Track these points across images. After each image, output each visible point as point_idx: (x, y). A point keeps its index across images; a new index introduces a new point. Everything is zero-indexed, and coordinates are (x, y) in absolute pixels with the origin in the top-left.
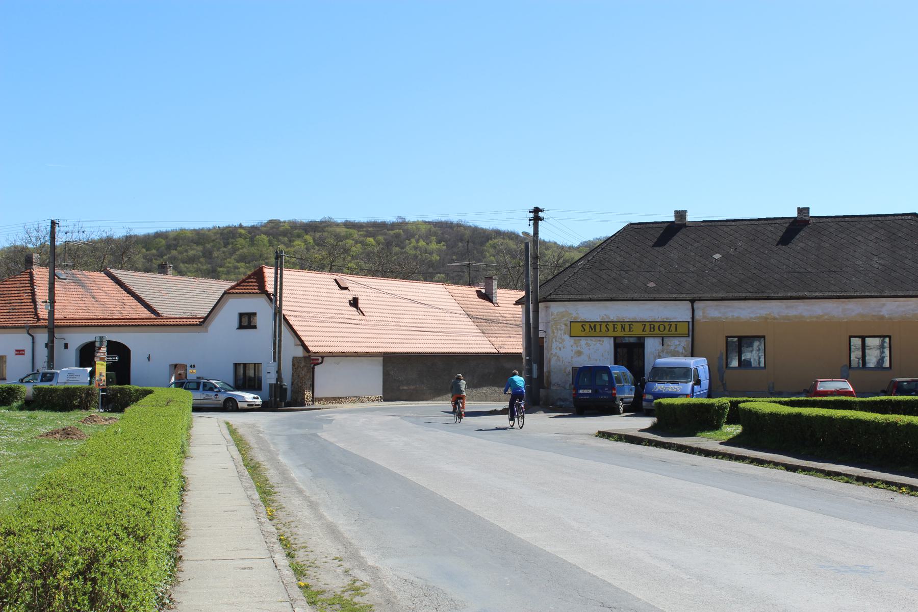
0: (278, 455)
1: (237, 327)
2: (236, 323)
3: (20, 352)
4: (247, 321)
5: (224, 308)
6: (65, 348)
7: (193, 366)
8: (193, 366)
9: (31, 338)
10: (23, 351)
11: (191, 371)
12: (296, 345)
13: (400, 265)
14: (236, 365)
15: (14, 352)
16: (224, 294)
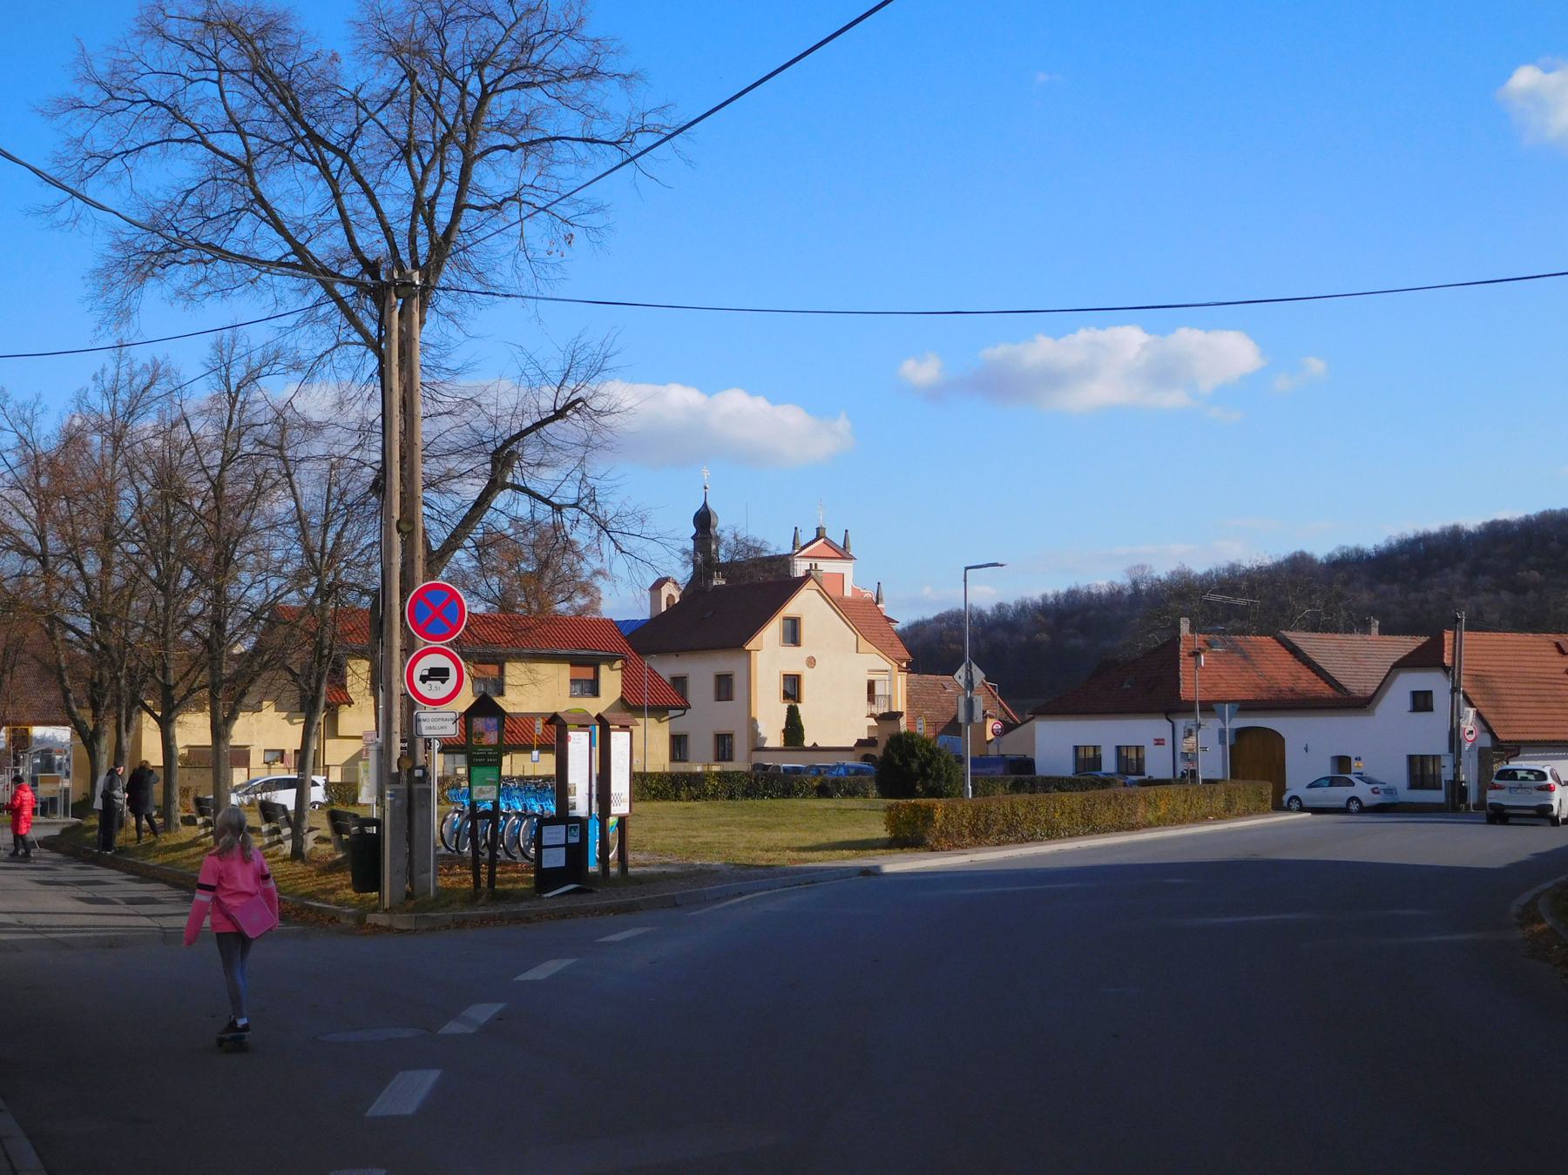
0: (1533, 932)
1: (1409, 709)
2: (1408, 706)
3: (1159, 742)
4: (1422, 702)
5: (1417, 674)
6: (718, 699)
7: (1358, 759)
8: (1358, 759)
9: (1171, 724)
10: (1163, 740)
11: (1356, 765)
12: (1482, 732)
13: (1110, 803)
14: (1411, 758)
15: (1153, 742)
16: (1393, 667)
